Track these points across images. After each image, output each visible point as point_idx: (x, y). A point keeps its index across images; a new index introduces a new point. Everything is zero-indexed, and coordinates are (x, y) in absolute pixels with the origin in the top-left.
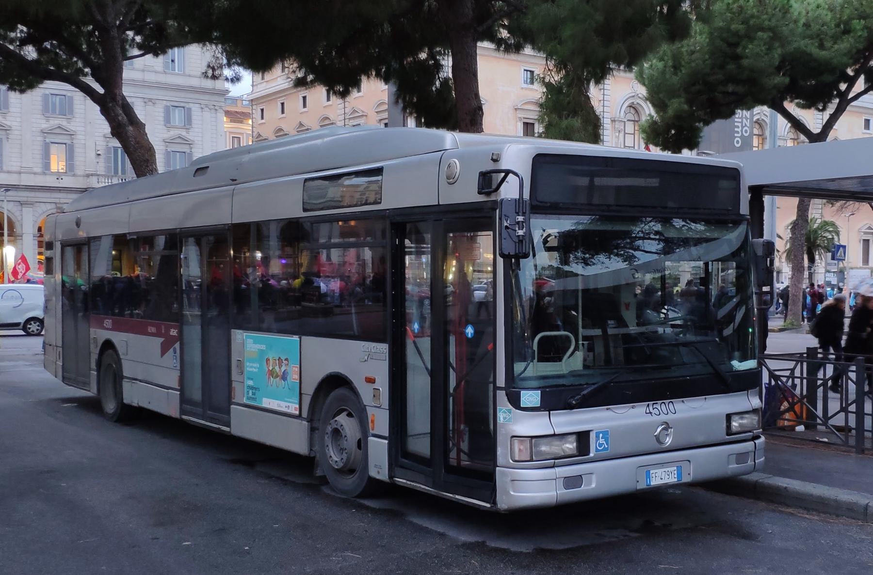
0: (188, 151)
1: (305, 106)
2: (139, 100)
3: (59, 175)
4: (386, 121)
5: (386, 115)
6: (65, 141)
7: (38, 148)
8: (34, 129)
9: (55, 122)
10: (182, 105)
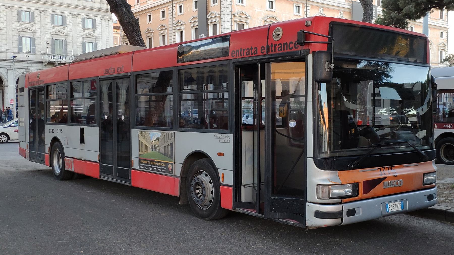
0: (64, 39)
1: (150, 20)
2: (69, 14)
3: (27, 54)
4: (197, 27)
5: (196, 24)
6: (62, 39)
7: (16, 40)
8: (13, 29)
9: (86, 32)
10: (91, 17)
